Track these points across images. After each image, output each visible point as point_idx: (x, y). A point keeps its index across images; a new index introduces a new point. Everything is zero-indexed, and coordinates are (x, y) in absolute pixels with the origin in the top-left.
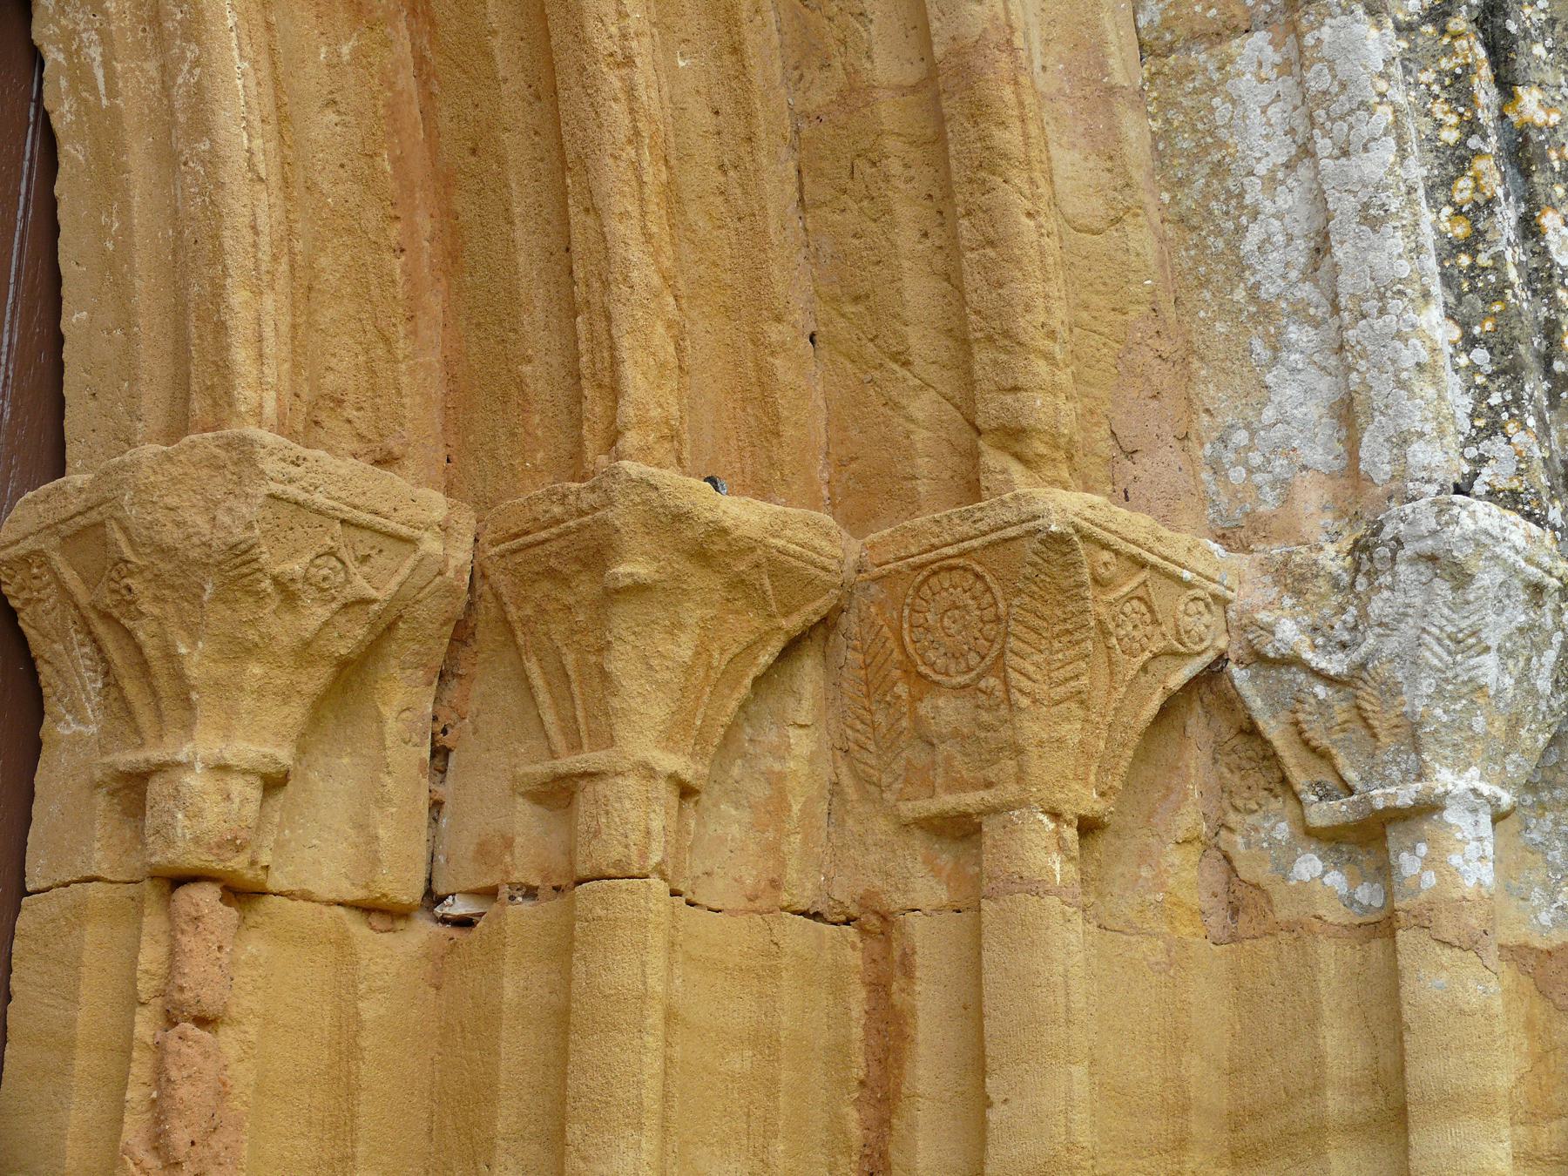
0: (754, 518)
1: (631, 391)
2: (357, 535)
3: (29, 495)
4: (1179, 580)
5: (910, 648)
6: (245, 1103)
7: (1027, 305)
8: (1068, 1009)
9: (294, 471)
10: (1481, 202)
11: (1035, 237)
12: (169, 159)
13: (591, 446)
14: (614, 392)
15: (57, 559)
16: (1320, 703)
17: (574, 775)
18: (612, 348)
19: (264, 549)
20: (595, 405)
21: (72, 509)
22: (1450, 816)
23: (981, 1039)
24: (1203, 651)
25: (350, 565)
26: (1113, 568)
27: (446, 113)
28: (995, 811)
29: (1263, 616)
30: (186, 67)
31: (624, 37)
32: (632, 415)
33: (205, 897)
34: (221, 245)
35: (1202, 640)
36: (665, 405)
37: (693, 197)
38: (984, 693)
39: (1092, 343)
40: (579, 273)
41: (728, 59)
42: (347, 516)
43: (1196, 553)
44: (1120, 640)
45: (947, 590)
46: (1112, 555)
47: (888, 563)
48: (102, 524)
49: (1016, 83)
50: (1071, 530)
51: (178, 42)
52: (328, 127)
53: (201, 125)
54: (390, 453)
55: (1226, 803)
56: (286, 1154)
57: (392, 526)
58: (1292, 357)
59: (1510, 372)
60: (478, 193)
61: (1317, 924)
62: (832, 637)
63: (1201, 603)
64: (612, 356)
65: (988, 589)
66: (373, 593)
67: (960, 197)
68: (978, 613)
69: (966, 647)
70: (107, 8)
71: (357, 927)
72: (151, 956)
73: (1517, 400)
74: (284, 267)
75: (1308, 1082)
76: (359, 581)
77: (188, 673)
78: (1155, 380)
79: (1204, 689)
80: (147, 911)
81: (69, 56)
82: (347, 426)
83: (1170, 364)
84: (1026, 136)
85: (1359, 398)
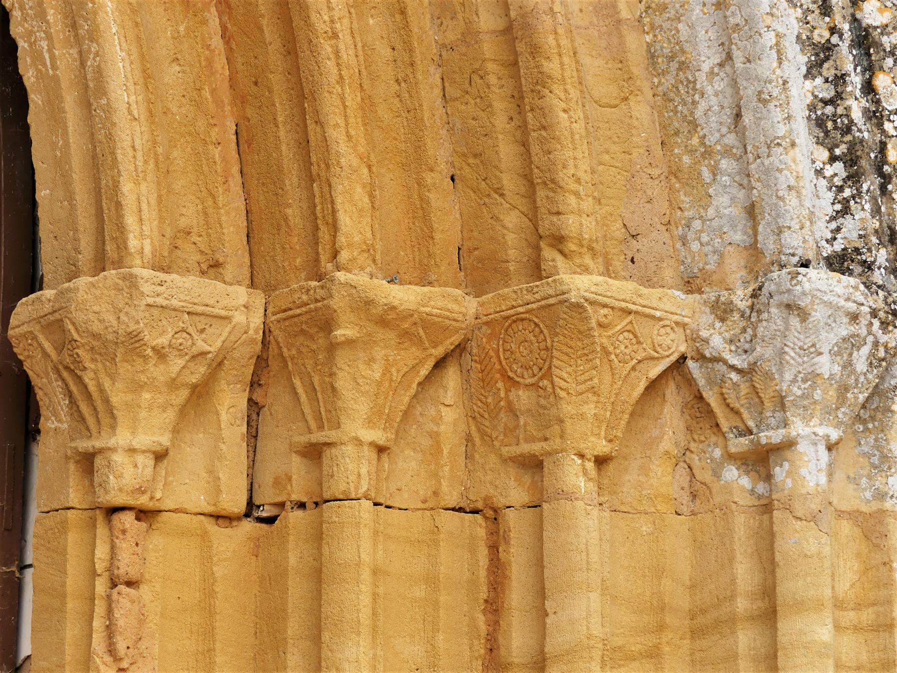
0: (412, 298)
1: (343, 228)
2: (197, 318)
3: (24, 299)
4: (653, 317)
5: (504, 363)
6: (156, 624)
7: (564, 164)
8: (588, 563)
9: (159, 289)
10: (839, 75)
11: (568, 124)
12: (86, 104)
13: (324, 258)
14: (335, 228)
15: (41, 338)
16: (735, 384)
17: (320, 444)
18: (333, 202)
19: (146, 333)
20: (324, 233)
21: (46, 311)
22: (801, 448)
23: (542, 581)
24: (671, 355)
25: (193, 334)
26: (610, 317)
27: (240, 60)
28: (549, 454)
29: (704, 334)
30: (92, 56)
31: (332, 22)
32: (344, 241)
33: (127, 519)
34: (116, 158)
35: (669, 348)
36: (363, 232)
37: (381, 101)
38: (542, 388)
39: (611, 173)
40: (314, 159)
41: (398, 17)
42: (191, 310)
43: (664, 299)
44: (617, 356)
45: (521, 331)
46: (610, 309)
47: (490, 314)
48: (62, 320)
49: (556, 33)
50: (582, 301)
51: (87, 42)
52: (174, 75)
53: (102, 90)
54: (217, 261)
55: (689, 437)
56: (179, 648)
57: (216, 311)
58: (724, 179)
59: (854, 178)
60: (260, 108)
61: (734, 506)
62: (463, 355)
63: (669, 328)
64: (333, 207)
65: (542, 332)
66: (208, 348)
67: (527, 100)
68: (537, 345)
69: (532, 363)
70: (48, 20)
71: (210, 525)
72: (102, 552)
73: (859, 193)
74: (151, 165)
75: (729, 593)
76: (200, 343)
77: (111, 400)
78: (649, 192)
79: (675, 372)
80: (98, 526)
81: (31, 45)
82: (193, 246)
83: (657, 182)
84: (562, 64)
85: (757, 205)
